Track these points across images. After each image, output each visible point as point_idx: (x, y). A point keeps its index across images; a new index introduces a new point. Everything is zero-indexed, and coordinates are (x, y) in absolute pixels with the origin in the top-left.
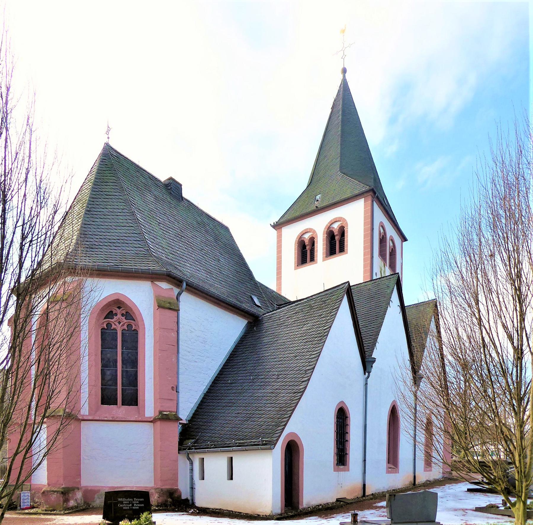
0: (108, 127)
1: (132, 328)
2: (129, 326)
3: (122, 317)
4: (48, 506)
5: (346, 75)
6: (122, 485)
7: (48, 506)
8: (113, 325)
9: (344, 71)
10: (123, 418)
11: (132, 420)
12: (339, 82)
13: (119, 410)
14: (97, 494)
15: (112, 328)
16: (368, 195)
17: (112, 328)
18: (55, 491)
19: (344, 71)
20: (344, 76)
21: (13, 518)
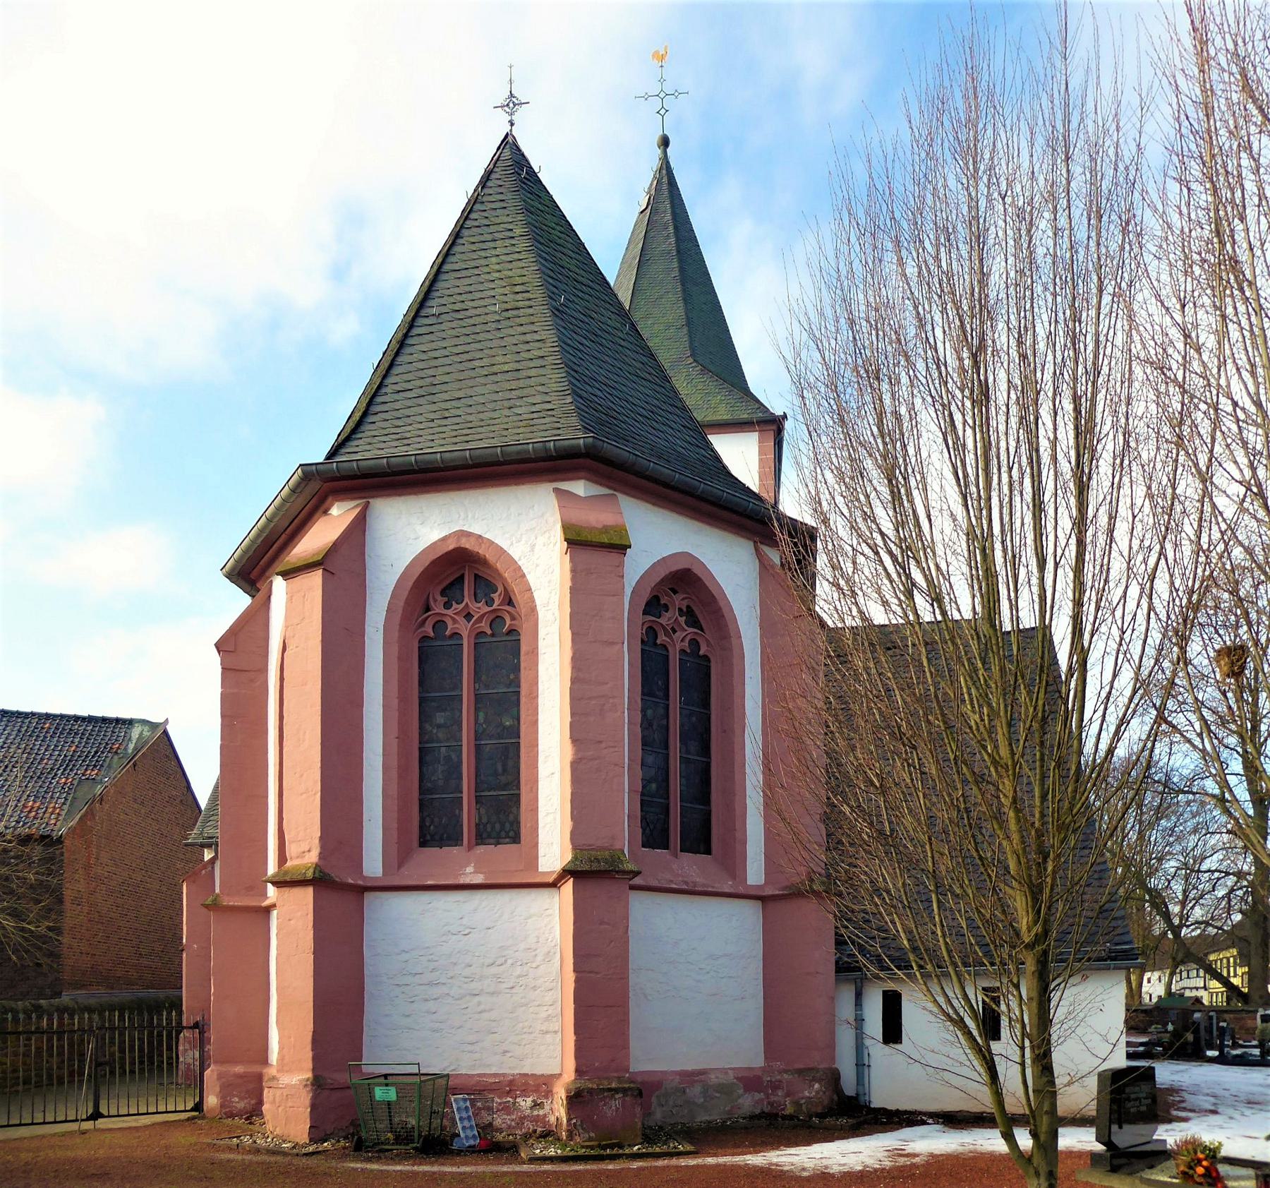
0: (511, 95)
1: (699, 650)
2: (695, 643)
3: (479, 605)
4: (592, 1135)
5: (668, 150)
6: (1001, 1078)
7: (592, 1135)
8: (450, 625)
9: (665, 142)
10: (704, 885)
11: (429, 882)
12: (656, 163)
13: (690, 867)
14: (657, 1093)
15: (448, 633)
16: (768, 428)
17: (448, 633)
18: (616, 1090)
19: (665, 142)
20: (665, 153)
21: (545, 1172)
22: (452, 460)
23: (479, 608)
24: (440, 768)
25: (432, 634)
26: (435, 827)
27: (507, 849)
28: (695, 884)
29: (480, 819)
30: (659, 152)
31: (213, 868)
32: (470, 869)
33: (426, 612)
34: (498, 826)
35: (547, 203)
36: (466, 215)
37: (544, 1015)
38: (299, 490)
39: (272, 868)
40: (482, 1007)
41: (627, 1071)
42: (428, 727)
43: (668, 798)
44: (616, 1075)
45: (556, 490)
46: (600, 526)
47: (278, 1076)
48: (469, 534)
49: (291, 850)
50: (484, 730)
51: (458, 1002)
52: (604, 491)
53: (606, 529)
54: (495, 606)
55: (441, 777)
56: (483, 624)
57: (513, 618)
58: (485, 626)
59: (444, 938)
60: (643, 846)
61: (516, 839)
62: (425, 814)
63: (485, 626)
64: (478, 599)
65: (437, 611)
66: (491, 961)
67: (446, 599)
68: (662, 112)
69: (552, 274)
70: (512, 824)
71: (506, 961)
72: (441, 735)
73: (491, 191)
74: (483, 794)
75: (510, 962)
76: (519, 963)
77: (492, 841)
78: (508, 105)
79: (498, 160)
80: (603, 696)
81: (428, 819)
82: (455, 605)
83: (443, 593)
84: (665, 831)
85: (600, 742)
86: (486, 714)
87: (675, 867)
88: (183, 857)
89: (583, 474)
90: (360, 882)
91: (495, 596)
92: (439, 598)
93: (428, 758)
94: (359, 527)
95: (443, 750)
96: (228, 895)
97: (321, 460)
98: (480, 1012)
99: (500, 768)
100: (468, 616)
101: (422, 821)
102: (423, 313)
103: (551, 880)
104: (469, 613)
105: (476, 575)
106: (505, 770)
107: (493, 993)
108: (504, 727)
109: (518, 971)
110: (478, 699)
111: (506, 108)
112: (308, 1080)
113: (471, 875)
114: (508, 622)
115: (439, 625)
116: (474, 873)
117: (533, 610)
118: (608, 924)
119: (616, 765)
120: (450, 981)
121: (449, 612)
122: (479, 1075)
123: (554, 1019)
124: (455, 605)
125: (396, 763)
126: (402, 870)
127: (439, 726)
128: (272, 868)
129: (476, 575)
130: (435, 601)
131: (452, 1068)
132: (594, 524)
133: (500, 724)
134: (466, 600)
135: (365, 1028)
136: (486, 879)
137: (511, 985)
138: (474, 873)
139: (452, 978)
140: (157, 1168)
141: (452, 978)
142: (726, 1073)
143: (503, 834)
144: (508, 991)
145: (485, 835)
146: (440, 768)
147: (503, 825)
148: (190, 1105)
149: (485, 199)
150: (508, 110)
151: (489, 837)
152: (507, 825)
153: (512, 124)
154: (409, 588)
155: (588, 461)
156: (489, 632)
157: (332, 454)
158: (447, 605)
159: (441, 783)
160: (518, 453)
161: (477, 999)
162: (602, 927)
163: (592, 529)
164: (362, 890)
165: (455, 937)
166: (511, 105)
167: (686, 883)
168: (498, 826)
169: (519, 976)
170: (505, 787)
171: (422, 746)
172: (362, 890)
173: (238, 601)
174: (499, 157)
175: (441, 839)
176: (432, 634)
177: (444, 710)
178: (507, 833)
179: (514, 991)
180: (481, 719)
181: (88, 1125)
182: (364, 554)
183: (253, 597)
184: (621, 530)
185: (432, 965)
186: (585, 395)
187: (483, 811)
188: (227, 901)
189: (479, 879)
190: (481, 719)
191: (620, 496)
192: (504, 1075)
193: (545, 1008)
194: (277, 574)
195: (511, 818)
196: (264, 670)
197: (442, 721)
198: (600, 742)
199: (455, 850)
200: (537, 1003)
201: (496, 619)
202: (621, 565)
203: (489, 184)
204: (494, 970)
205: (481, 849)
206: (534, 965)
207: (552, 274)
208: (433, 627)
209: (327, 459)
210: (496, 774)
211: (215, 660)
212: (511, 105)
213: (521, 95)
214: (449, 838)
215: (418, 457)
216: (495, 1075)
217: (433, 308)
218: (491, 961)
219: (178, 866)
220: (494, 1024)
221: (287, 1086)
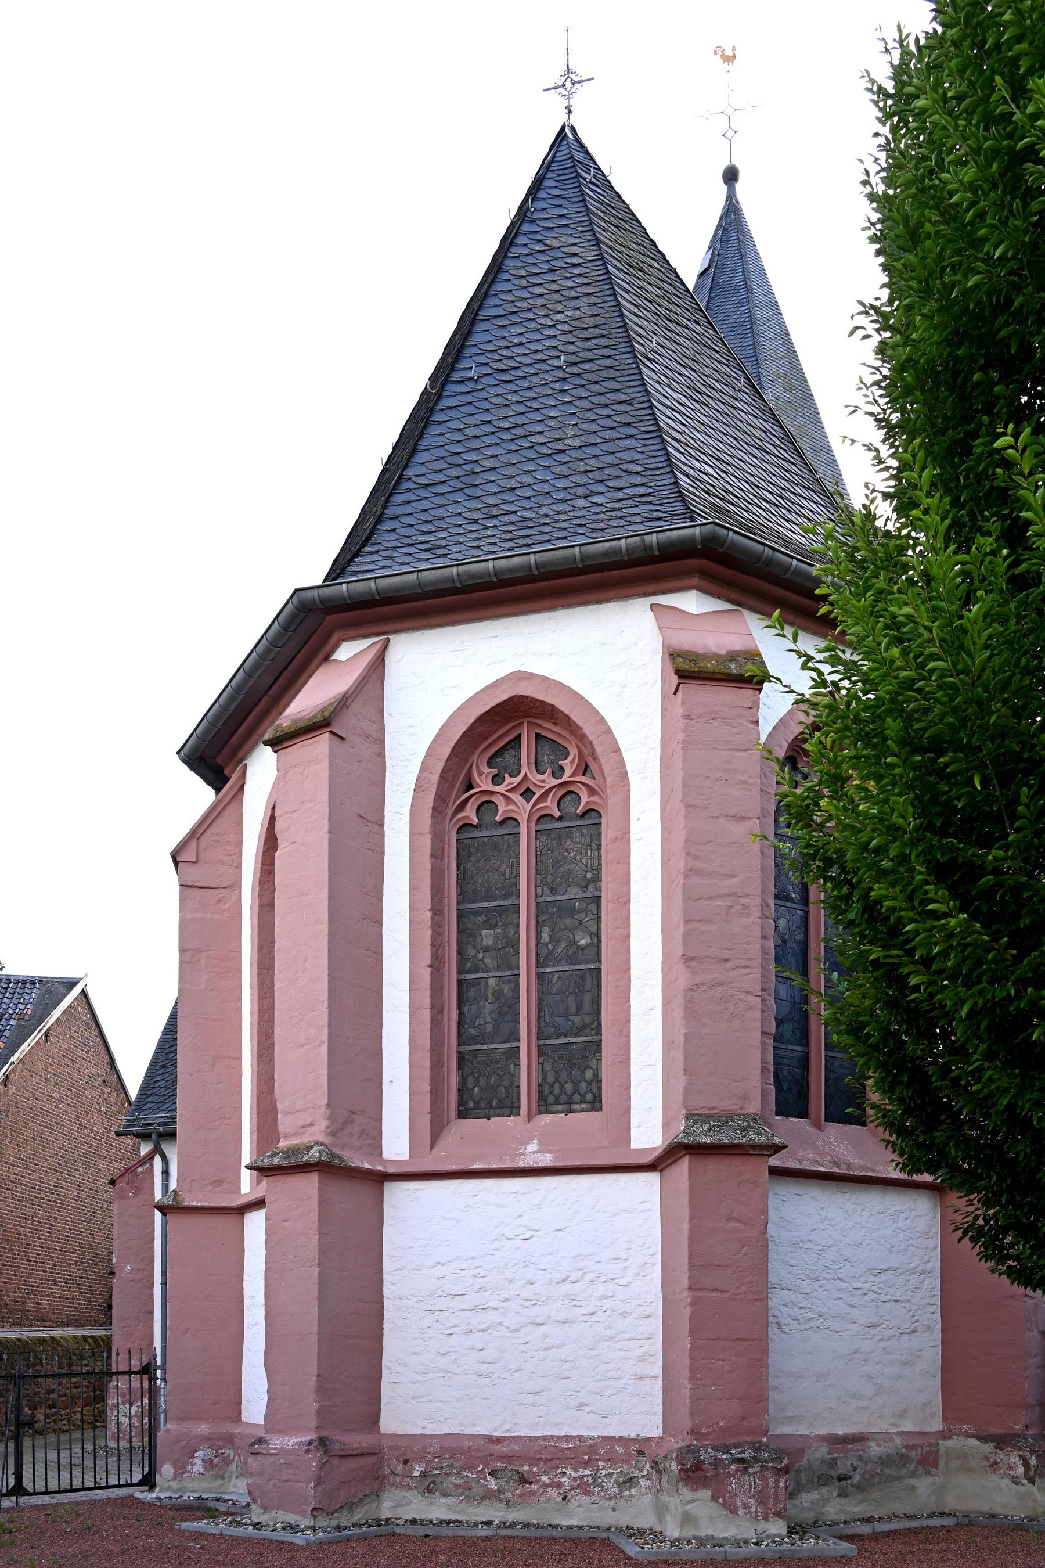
5: (739, 186)
8: (502, 806)
9: (731, 176)
10: (861, 1168)
19: (731, 176)
22: (511, 570)
23: (543, 781)
24: (488, 1007)
25: (475, 821)
26: (481, 1090)
27: (582, 1119)
28: (849, 1165)
29: (544, 1078)
30: (724, 188)
31: (152, 1165)
32: (532, 1147)
33: (467, 791)
34: (569, 1087)
35: (626, 216)
36: (508, 241)
37: (639, 1352)
38: (291, 629)
39: (158, 1195)
40: (549, 1342)
41: (765, 1433)
42: (471, 951)
43: (807, 1045)
44: (749, 1439)
45: (653, 607)
46: (723, 652)
47: (268, 1437)
48: (530, 677)
49: (285, 1123)
50: (550, 953)
51: (514, 1334)
52: (728, 606)
53: (732, 656)
54: (565, 778)
55: (489, 1020)
56: (548, 804)
57: (592, 791)
58: (550, 805)
59: (496, 1245)
60: (777, 1114)
61: (596, 1104)
62: (467, 1071)
63: (550, 805)
64: (541, 769)
65: (484, 788)
66: (563, 1277)
67: (495, 771)
68: (729, 134)
69: (636, 310)
70: (589, 1083)
71: (582, 1277)
72: (488, 961)
73: (543, 205)
74: (548, 1042)
75: (590, 1276)
76: (603, 1279)
77: (560, 1107)
78: (564, 85)
79: (552, 161)
80: (730, 895)
81: (471, 1079)
82: (508, 779)
83: (490, 764)
84: (803, 1094)
85: (726, 960)
86: (552, 930)
87: (819, 1141)
88: (105, 1154)
89: (695, 581)
90: (379, 1168)
91: (566, 763)
92: (486, 769)
93: (471, 993)
94: (378, 665)
95: (492, 982)
96: (190, 1192)
97: (319, 582)
98: (546, 1349)
99: (573, 1008)
100: (527, 794)
101: (463, 1080)
102: (456, 376)
103: (647, 1159)
104: (528, 789)
105: (538, 735)
106: (579, 1008)
107: (565, 1322)
108: (579, 947)
109: (601, 1289)
110: (541, 909)
111: (576, 79)
112: (310, 1443)
113: (533, 1154)
114: (584, 799)
115: (486, 806)
116: (539, 1151)
117: (623, 777)
118: (739, 1221)
119: (749, 993)
120: (505, 1305)
121: (501, 789)
122: (544, 1438)
123: (652, 1359)
124: (508, 779)
125: (428, 1001)
126: (434, 1150)
127: (486, 949)
128: (158, 1195)
129: (538, 735)
130: (480, 774)
131: (507, 1426)
132: (714, 649)
133: (574, 943)
134: (524, 770)
135: (385, 1372)
136: (556, 1159)
137: (590, 1310)
138: (539, 1151)
139: (506, 1300)
140: (824, 1560)
141: (506, 1300)
142: (891, 1440)
143: (577, 1097)
144: (585, 1318)
145: (551, 1099)
146: (488, 1007)
147: (576, 1084)
148: (137, 1478)
149: (536, 216)
150: (564, 92)
151: (557, 1102)
152: (583, 1085)
153: (570, 112)
154: (446, 757)
155: (704, 563)
156: (557, 814)
157: (339, 569)
158: (497, 779)
159: (489, 1028)
160: (605, 554)
161: (542, 1329)
162: (730, 1225)
163: (706, 657)
164: (381, 1178)
165: (511, 1242)
166: (569, 84)
167: (836, 1164)
168: (569, 1087)
169: (601, 1298)
170: (579, 1031)
171: (462, 977)
172: (381, 1178)
173: (201, 795)
174: (554, 157)
175: (490, 1106)
176: (475, 821)
177: (494, 927)
178: (583, 1096)
179: (594, 1318)
180: (545, 937)
181: (139, 1493)
182: (381, 711)
183: (218, 790)
184: (754, 656)
185: (478, 1283)
186: (692, 472)
187: (548, 1067)
188: (190, 1201)
189: (546, 1160)
190: (545, 937)
191: (746, 613)
192: (580, 1438)
193: (640, 1343)
194: (266, 743)
195: (589, 1074)
196: (235, 886)
197: (491, 942)
198: (726, 960)
199: (510, 1121)
200: (628, 1336)
201: (567, 793)
202: (756, 705)
203: (542, 194)
204: (566, 1288)
205: (547, 1119)
206: (623, 1282)
207: (636, 310)
208: (477, 812)
209: (324, 581)
210: (566, 1014)
211: (170, 880)
212: (569, 84)
213: (582, 70)
214: (501, 1105)
215: (460, 568)
216: (568, 1438)
217: (469, 367)
218: (560, 1276)
219: (100, 1166)
220: (566, 1365)
221: (283, 1451)
